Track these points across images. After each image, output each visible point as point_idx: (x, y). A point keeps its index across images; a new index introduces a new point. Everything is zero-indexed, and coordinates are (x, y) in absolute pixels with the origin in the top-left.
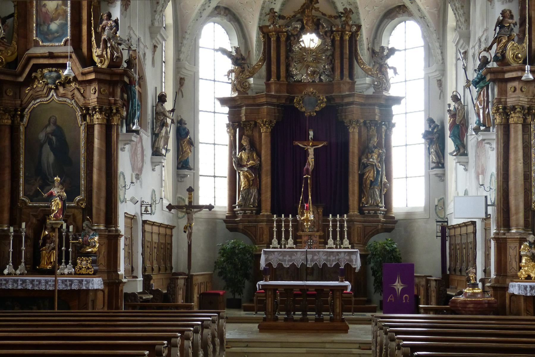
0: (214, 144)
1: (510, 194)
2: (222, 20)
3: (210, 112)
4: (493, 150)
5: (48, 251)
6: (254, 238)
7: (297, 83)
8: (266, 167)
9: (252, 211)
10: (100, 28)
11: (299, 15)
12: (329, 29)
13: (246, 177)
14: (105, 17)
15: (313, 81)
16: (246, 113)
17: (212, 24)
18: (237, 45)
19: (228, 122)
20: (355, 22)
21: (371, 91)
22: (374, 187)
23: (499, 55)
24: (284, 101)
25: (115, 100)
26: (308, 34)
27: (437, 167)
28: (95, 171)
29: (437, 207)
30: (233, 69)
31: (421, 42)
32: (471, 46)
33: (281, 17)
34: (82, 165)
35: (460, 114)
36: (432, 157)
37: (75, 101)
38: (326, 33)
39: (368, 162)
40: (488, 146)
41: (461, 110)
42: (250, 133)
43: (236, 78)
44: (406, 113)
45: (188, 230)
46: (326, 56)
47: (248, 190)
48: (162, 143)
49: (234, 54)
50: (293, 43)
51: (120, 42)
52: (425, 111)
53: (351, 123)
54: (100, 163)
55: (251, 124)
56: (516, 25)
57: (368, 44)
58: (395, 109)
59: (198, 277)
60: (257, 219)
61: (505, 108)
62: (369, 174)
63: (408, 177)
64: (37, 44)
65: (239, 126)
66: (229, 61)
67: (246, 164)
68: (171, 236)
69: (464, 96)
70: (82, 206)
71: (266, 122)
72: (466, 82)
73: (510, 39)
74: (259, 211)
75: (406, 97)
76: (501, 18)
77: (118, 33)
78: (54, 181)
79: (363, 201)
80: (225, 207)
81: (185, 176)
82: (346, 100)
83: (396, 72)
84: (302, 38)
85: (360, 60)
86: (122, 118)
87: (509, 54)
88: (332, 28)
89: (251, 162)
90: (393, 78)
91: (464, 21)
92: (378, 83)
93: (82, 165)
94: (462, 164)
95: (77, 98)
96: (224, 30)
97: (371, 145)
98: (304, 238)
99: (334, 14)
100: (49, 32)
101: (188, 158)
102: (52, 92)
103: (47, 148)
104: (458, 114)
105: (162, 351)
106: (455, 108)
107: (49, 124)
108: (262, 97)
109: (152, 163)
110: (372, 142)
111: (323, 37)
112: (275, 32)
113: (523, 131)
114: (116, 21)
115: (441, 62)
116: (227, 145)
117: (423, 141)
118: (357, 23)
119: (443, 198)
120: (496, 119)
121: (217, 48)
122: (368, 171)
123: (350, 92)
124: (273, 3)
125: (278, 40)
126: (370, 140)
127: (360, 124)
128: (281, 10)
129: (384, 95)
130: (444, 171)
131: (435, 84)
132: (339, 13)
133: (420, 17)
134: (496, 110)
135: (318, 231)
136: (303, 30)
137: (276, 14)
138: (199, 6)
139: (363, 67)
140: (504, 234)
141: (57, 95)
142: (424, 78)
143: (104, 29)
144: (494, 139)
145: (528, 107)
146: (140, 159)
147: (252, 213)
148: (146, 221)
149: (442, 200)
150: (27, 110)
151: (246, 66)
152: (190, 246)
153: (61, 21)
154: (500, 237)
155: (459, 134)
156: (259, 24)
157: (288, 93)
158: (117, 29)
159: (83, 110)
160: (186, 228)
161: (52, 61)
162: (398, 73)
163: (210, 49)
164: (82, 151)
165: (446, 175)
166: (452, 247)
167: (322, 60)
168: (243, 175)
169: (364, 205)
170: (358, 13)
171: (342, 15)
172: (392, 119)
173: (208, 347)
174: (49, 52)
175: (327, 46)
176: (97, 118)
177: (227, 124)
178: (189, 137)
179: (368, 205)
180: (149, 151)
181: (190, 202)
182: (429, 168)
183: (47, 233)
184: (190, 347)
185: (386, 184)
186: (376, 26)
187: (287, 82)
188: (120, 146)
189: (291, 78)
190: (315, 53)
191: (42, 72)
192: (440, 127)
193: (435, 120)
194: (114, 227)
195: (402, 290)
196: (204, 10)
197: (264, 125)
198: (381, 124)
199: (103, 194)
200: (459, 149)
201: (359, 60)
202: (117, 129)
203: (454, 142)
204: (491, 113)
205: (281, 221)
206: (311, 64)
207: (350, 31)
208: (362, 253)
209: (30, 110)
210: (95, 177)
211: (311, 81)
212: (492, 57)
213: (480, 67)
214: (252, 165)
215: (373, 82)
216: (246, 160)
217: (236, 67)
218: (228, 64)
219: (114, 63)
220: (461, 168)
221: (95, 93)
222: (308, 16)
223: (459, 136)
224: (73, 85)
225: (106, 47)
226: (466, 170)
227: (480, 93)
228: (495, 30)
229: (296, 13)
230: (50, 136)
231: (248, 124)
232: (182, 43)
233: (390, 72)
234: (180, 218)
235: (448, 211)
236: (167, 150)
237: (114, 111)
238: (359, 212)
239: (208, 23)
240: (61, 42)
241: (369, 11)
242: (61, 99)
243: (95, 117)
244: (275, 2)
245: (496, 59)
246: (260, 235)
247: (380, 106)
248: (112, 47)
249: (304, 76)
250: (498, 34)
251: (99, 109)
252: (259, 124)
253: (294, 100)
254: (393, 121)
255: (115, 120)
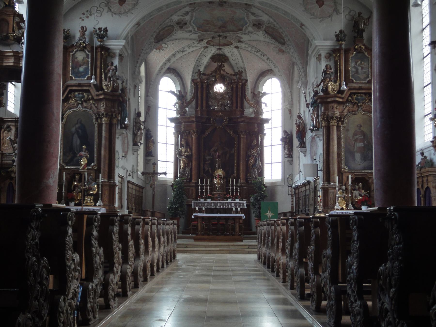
1: (330, 164)
2: (172, 76)
4: (321, 141)
5: (76, 193)
10: (107, 71)
11: (214, 74)
13: (184, 161)
14: (110, 64)
16: (184, 126)
17: (166, 78)
18: (179, 89)
19: (174, 131)
21: (253, 116)
23: (324, 88)
24: (205, 120)
25: (114, 110)
26: (219, 84)
28: (103, 149)
31: (280, 90)
32: (308, 88)
33: (204, 74)
34: (96, 146)
35: (302, 125)
37: (92, 111)
40: (318, 138)
42: (186, 137)
46: (228, 96)
47: (184, 168)
48: (138, 139)
49: (178, 94)
51: (118, 78)
54: (105, 145)
56: (333, 73)
58: (266, 126)
59: (158, 214)
61: (327, 118)
63: (273, 163)
64: (71, 79)
65: (180, 134)
68: (142, 192)
69: (304, 116)
70: (96, 169)
73: (330, 80)
74: (191, 180)
75: (272, 119)
76: (325, 69)
77: (117, 73)
78: (82, 148)
80: (172, 179)
82: (240, 120)
83: (266, 106)
86: (118, 120)
87: (330, 88)
89: (187, 153)
93: (96, 146)
95: (93, 109)
99: (233, 73)
100: (79, 72)
102: (80, 106)
103: (76, 136)
106: (299, 122)
107: (77, 123)
108: (193, 118)
109: (133, 150)
113: (337, 130)
114: (116, 67)
115: (291, 100)
116: (173, 145)
117: (281, 143)
120: (323, 123)
125: (202, 86)
128: (204, 71)
130: (293, 159)
131: (288, 112)
134: (322, 119)
136: (216, 82)
140: (327, 186)
141: (82, 107)
142: (282, 109)
143: (109, 71)
144: (321, 135)
145: (340, 117)
146: (126, 146)
147: (187, 181)
148: (130, 181)
149: (291, 175)
150: (65, 115)
152: (154, 195)
153: (85, 67)
154: (325, 187)
156: (192, 78)
158: (116, 71)
159: (96, 115)
160: (152, 185)
161: (80, 88)
164: (96, 138)
165: (293, 161)
166: (297, 200)
167: (226, 98)
168: (182, 160)
170: (246, 73)
171: (237, 74)
174: (78, 83)
176: (104, 120)
177: (174, 132)
180: (131, 143)
181: (154, 171)
182: (284, 157)
183: (75, 183)
184: (161, 229)
186: (255, 82)
188: (117, 136)
190: (222, 95)
191: (74, 94)
193: (288, 131)
194: (113, 180)
196: (162, 69)
197: (194, 133)
199: (107, 162)
202: (115, 126)
204: (320, 120)
205: (203, 186)
209: (67, 115)
210: (103, 152)
212: (321, 90)
213: (314, 96)
215: (254, 111)
217: (179, 101)
218: (174, 99)
219: (115, 90)
220: (302, 155)
221: (103, 106)
222: (219, 74)
224: (91, 101)
225: (110, 81)
226: (305, 156)
227: (314, 110)
228: (322, 75)
230: (78, 130)
232: (149, 87)
233: (263, 105)
236: (141, 144)
237: (114, 116)
239: (164, 77)
240: (85, 78)
242: (84, 109)
243: (103, 119)
245: (323, 91)
247: (258, 124)
248: (114, 81)
250: (324, 77)
251: (106, 115)
254: (265, 132)
255: (115, 121)
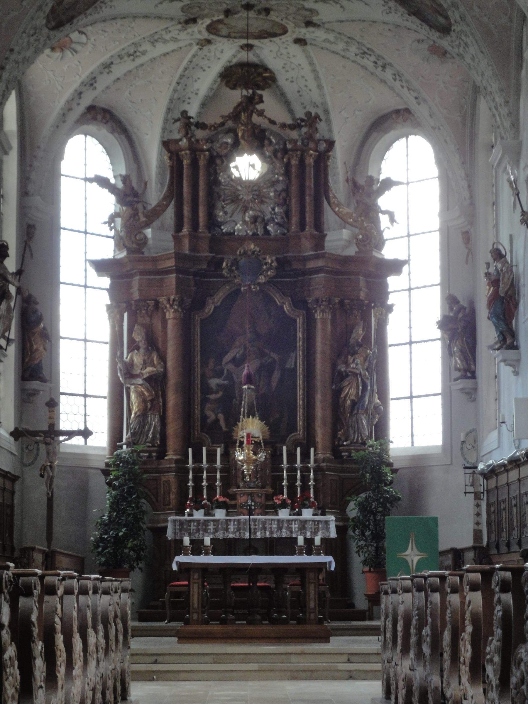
0: (85, 340)
3: (79, 285)
6: (154, 500)
7: (226, 237)
8: (173, 379)
9: (150, 452)
12: (282, 146)
13: (141, 395)
15: (254, 234)
16: (141, 285)
20: (323, 137)
21: (352, 251)
22: (358, 411)
26: (246, 155)
27: (465, 377)
29: (464, 445)
30: (118, 211)
35: (506, 280)
36: (455, 360)
38: (275, 152)
39: (349, 369)
41: (508, 273)
42: (147, 320)
43: (125, 226)
44: (410, 289)
45: (48, 473)
46: (275, 191)
47: (143, 416)
49: (120, 185)
50: (219, 169)
52: (442, 284)
53: (320, 303)
55: (149, 306)
57: (347, 172)
60: (161, 466)
62: (349, 389)
65: (128, 308)
66: (111, 199)
67: (140, 373)
68: (13, 493)
71: (174, 300)
72: (520, 214)
74: (162, 452)
79: (339, 436)
81: (35, 393)
83: (392, 220)
84: (234, 161)
85: (334, 198)
88: (285, 144)
90: (389, 228)
91: (510, 127)
92: (363, 237)
94: (512, 363)
96: (101, 147)
97: (352, 341)
98: (239, 498)
101: (41, 361)
104: (503, 280)
105: (55, 585)
106: (497, 270)
110: (354, 335)
111: (271, 159)
112: (189, 149)
117: (438, 333)
118: (327, 137)
119: (474, 430)
121: (91, 175)
122: (349, 384)
123: (316, 251)
124: (186, 103)
126: (351, 332)
127: (335, 304)
128: (199, 114)
129: (374, 256)
130: (476, 383)
132: (298, 119)
133: (432, 127)
135: (263, 487)
137: (192, 120)
138: (60, 103)
139: (339, 210)
147: (150, 456)
151: (140, 206)
152: (50, 501)
155: (504, 313)
156: (162, 137)
157: (211, 252)
162: (398, 221)
163: (77, 178)
166: (492, 509)
168: (136, 391)
169: (341, 442)
170: (328, 121)
171: (303, 124)
172: (387, 298)
173: (109, 625)
175: (277, 174)
178: (42, 325)
179: (349, 442)
185: (378, 407)
187: (209, 235)
189: (217, 229)
192: (467, 311)
193: (460, 298)
195: (419, 562)
196: (70, 109)
197: (172, 306)
198: (369, 308)
200: (504, 339)
201: (331, 199)
203: (495, 326)
205: (201, 470)
206: (251, 205)
207: (316, 151)
208: (338, 523)
211: (251, 233)
214: (152, 374)
215: (356, 237)
216: (141, 366)
217: (124, 208)
222: (246, 125)
223: (504, 316)
226: (516, 373)
229: (226, 118)
231: (144, 306)
232: (31, 166)
233: (384, 220)
234: (26, 465)
235: (485, 444)
238: (333, 455)
241: (348, 118)
244: (189, 101)
246: (164, 493)
249: (238, 225)
252: (163, 304)
253: (222, 264)
254: (389, 302)
